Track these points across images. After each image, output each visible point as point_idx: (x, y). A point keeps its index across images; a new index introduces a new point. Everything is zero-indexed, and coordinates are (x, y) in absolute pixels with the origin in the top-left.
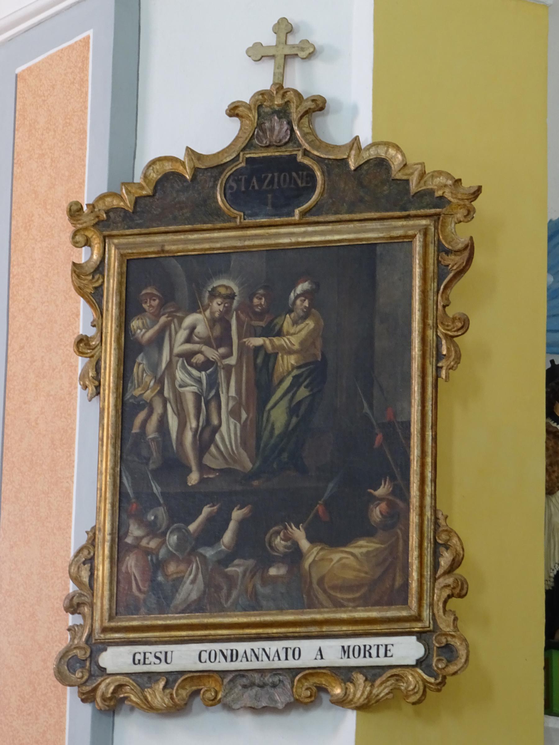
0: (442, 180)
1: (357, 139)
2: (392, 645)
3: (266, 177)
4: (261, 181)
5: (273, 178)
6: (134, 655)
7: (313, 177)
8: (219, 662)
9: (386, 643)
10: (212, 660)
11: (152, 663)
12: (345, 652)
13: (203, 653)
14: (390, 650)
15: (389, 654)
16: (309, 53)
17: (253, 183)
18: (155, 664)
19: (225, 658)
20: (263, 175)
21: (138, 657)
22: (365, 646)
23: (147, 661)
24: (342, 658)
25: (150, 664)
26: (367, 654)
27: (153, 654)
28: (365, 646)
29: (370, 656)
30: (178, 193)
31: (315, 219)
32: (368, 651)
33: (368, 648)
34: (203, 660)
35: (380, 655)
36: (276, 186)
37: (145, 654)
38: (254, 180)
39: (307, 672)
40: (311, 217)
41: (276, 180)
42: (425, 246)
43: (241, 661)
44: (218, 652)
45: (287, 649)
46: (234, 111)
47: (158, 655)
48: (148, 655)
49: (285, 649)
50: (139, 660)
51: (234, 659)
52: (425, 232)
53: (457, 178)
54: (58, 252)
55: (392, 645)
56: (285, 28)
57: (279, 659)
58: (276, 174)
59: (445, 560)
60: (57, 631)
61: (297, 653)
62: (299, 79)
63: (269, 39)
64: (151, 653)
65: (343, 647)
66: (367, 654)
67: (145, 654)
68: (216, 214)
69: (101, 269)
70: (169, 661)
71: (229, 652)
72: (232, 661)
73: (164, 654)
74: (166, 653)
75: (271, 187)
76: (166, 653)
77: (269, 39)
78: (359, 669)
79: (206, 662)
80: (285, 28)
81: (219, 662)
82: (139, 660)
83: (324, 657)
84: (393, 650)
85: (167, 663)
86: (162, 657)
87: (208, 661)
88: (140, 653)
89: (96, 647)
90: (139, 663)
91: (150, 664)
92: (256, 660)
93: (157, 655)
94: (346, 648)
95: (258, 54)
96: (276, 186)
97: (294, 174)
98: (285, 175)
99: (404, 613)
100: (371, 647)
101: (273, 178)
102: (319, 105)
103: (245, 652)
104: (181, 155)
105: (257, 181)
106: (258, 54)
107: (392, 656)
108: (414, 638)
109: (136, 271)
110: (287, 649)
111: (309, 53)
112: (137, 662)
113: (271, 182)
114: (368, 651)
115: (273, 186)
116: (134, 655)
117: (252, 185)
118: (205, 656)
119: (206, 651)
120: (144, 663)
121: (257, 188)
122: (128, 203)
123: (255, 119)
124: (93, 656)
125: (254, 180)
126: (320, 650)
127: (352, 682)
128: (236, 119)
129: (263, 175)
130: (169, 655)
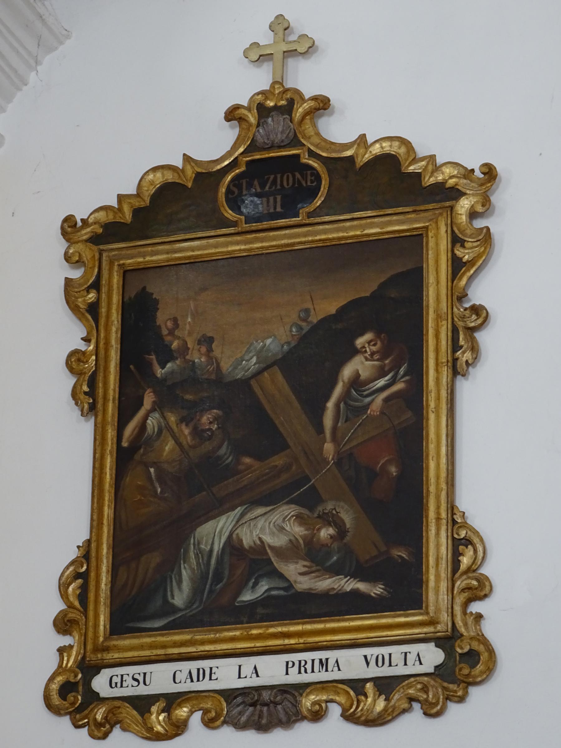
0: (448, 170)
2: (217, 667)
3: (268, 179)
5: (275, 180)
7: (318, 178)
13: (114, 678)
14: (215, 673)
15: (214, 677)
16: (308, 49)
20: (266, 177)
21: (115, 680)
22: (300, 662)
23: (125, 684)
24: (320, 671)
25: (246, 677)
26: (303, 669)
27: (131, 676)
28: (300, 662)
29: (306, 672)
31: (318, 220)
32: (304, 666)
33: (303, 663)
35: (315, 670)
36: (279, 187)
37: (122, 676)
46: (233, 114)
47: (136, 676)
49: (403, 654)
50: (116, 683)
53: (469, 168)
54: (50, 269)
55: (217, 667)
56: (281, 26)
57: (192, 681)
58: (279, 176)
59: (465, 561)
62: (307, 79)
63: (265, 38)
64: (128, 675)
66: (303, 669)
67: (122, 676)
70: (147, 683)
72: (198, 680)
73: (142, 675)
75: (274, 188)
76: (145, 674)
77: (265, 38)
80: (281, 26)
82: (116, 683)
83: (259, 675)
84: (217, 674)
85: (175, 682)
86: (141, 679)
88: (117, 676)
89: (89, 669)
90: (116, 686)
91: (246, 677)
93: (135, 677)
94: (324, 661)
95: (258, 56)
97: (298, 175)
98: (288, 177)
100: (306, 662)
101: (275, 180)
102: (322, 104)
103: (190, 673)
104: (178, 163)
105: (260, 184)
106: (258, 56)
108: (433, 644)
111: (308, 49)
112: (113, 685)
113: (274, 182)
114: (304, 666)
115: (276, 187)
120: (122, 686)
122: (128, 217)
124: (87, 681)
129: (266, 177)
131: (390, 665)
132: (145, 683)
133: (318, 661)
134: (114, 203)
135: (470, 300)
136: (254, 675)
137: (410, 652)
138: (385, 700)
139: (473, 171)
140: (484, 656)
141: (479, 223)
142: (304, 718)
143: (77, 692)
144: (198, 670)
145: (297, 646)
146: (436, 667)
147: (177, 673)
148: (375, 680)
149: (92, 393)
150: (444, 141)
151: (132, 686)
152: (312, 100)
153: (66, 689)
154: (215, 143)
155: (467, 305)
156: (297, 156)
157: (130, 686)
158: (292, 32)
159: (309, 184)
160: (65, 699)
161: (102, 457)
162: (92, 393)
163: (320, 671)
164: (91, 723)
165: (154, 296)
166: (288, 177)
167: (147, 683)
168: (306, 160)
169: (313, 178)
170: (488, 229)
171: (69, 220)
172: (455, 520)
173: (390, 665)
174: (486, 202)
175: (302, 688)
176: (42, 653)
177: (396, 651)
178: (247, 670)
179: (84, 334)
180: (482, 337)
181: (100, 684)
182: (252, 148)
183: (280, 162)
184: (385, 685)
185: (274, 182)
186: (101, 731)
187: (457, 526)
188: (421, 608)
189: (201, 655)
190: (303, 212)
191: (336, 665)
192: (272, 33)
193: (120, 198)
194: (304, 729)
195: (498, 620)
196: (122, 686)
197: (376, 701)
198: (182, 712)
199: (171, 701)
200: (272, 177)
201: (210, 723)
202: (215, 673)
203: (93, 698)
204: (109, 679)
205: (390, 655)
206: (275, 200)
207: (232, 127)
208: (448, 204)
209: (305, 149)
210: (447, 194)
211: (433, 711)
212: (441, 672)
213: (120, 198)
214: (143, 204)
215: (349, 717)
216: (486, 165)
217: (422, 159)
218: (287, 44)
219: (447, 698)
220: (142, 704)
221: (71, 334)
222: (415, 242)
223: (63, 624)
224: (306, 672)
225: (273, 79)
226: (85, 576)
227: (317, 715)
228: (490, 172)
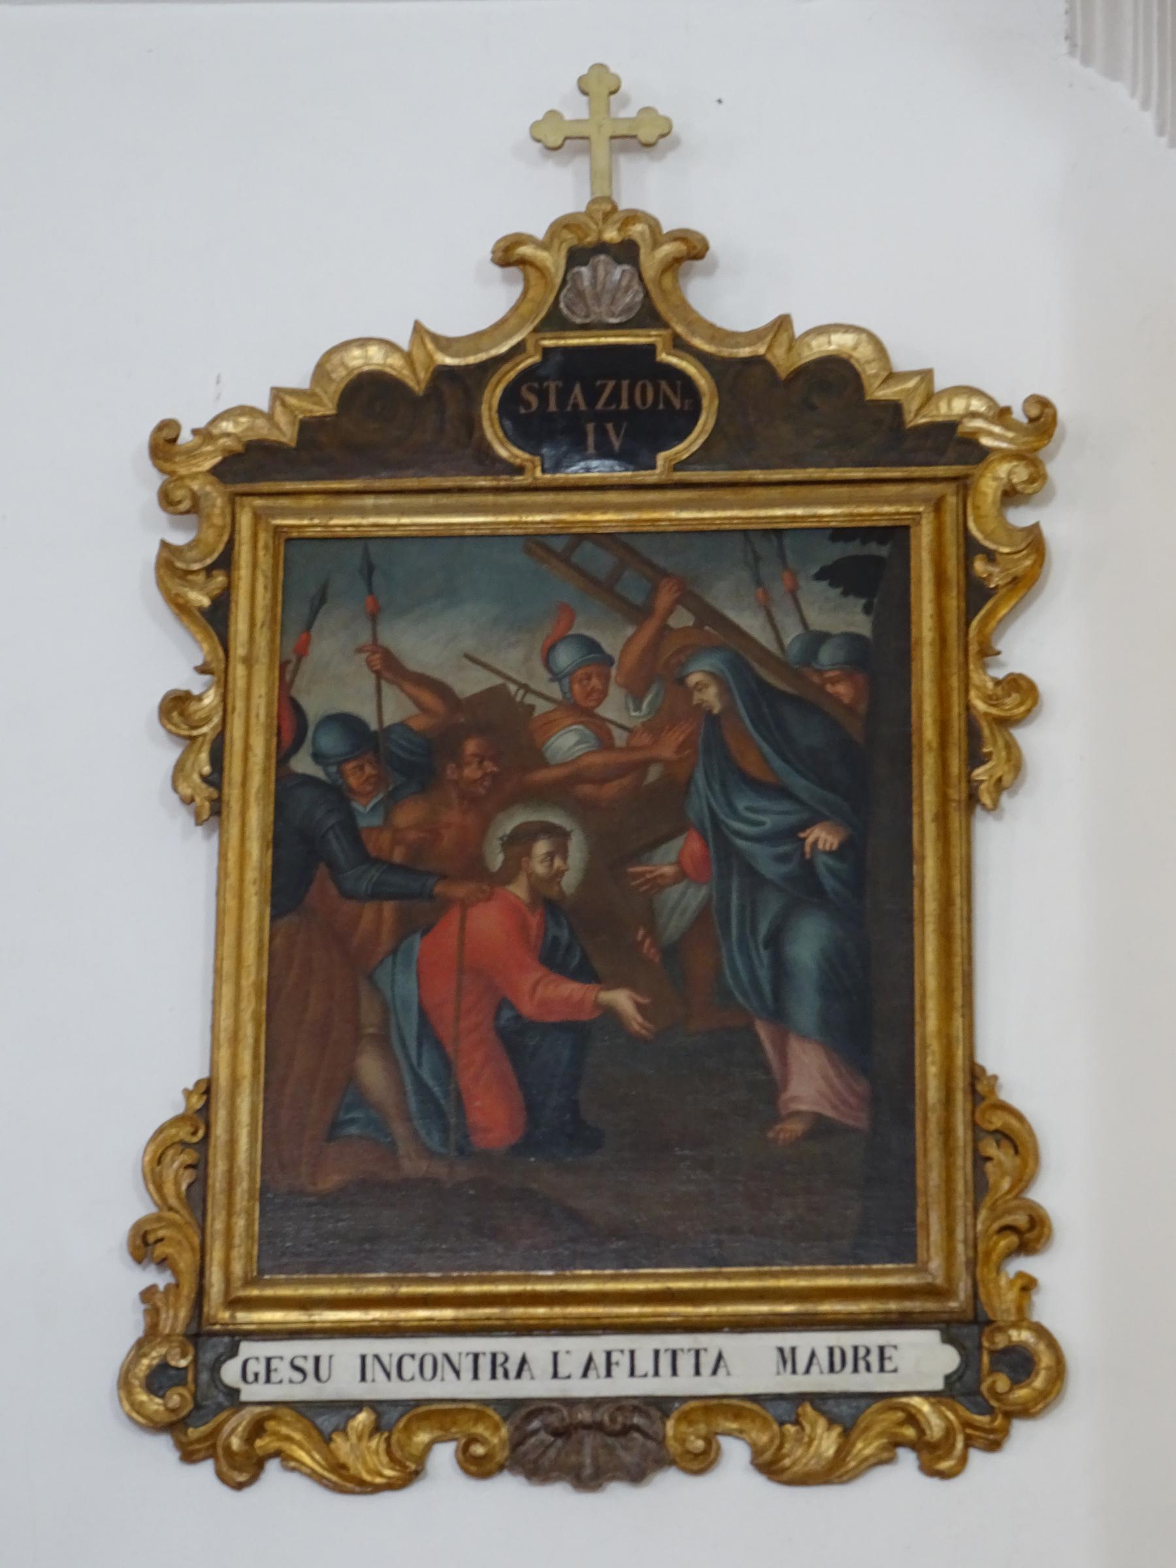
2: (895, 1347)
3: (604, 387)
4: (592, 396)
5: (617, 391)
9: (269, 1354)
12: (785, 1362)
14: (617, 1364)
15: (888, 1366)
16: (647, 138)
17: (575, 398)
18: (291, 1381)
19: (388, 1375)
21: (252, 1367)
22: (856, 1349)
23: (275, 1377)
24: (778, 1373)
28: (856, 1349)
29: (506, 1375)
30: (378, 420)
32: (502, 1364)
33: (862, 1352)
34: (562, 1371)
36: (624, 405)
38: (577, 389)
39: (693, 1404)
41: (625, 395)
42: (939, 531)
44: (440, 1359)
45: (476, 1357)
46: (508, 255)
47: (299, 1362)
48: (275, 1364)
50: (256, 1375)
52: (938, 506)
55: (895, 1347)
56: (599, 85)
58: (625, 384)
61: (787, 1358)
62: (659, 194)
63: (576, 109)
65: (781, 1350)
66: (862, 1365)
67: (268, 1361)
69: (559, 545)
74: (317, 1359)
75: (613, 407)
76: (317, 1359)
78: (817, 1399)
79: (413, 1379)
80: (599, 85)
82: (256, 1375)
84: (896, 1359)
86: (309, 1366)
95: (556, 140)
96: (624, 405)
97: (664, 385)
99: (911, 1280)
100: (868, 1352)
101: (617, 391)
102: (693, 249)
106: (556, 140)
107: (895, 1371)
111: (647, 138)
112: (250, 1377)
113: (615, 397)
117: (571, 402)
118: (410, 1367)
119: (413, 1356)
120: (268, 1380)
121: (583, 406)
122: (287, 434)
123: (557, 270)
125: (577, 389)
127: (797, 1422)
128: (514, 271)
134: (263, 404)
135: (1001, 665)
137: (705, 1350)
138: (841, 1435)
139: (1006, 411)
140: (1045, 1359)
141: (1021, 517)
142: (672, 1462)
144: (831, 1351)
146: (948, 1378)
148: (374, 1405)
149: (215, 779)
151: (291, 1381)
152: (676, 239)
153: (160, 1379)
154: (470, 305)
155: (1000, 674)
156: (651, 349)
157: (286, 1380)
158: (625, 103)
161: (946, 903)
162: (215, 779)
163: (778, 1373)
164: (220, 1451)
165: (839, 590)
166: (644, 388)
170: (1036, 526)
174: (1038, 476)
175: (661, 1405)
176: (108, 1306)
177: (538, 1348)
178: (572, 1365)
179: (199, 662)
180: (1026, 737)
182: (554, 321)
183: (610, 357)
185: (615, 397)
186: (241, 1470)
187: (983, 1105)
188: (914, 1259)
192: (585, 99)
193: (278, 394)
194: (670, 1485)
195: (1066, 1291)
196: (268, 1380)
197: (814, 1439)
199: (390, 1417)
200: (611, 384)
201: (477, 1467)
202: (617, 1364)
207: (508, 280)
210: (952, 446)
213: (278, 394)
214: (319, 411)
215: (770, 1466)
216: (1044, 403)
218: (607, 126)
219: (969, 1443)
220: (323, 1417)
221: (173, 659)
223: (143, 1245)
224: (506, 1375)
225: (592, 194)
227: (701, 1462)
228: (1042, 420)
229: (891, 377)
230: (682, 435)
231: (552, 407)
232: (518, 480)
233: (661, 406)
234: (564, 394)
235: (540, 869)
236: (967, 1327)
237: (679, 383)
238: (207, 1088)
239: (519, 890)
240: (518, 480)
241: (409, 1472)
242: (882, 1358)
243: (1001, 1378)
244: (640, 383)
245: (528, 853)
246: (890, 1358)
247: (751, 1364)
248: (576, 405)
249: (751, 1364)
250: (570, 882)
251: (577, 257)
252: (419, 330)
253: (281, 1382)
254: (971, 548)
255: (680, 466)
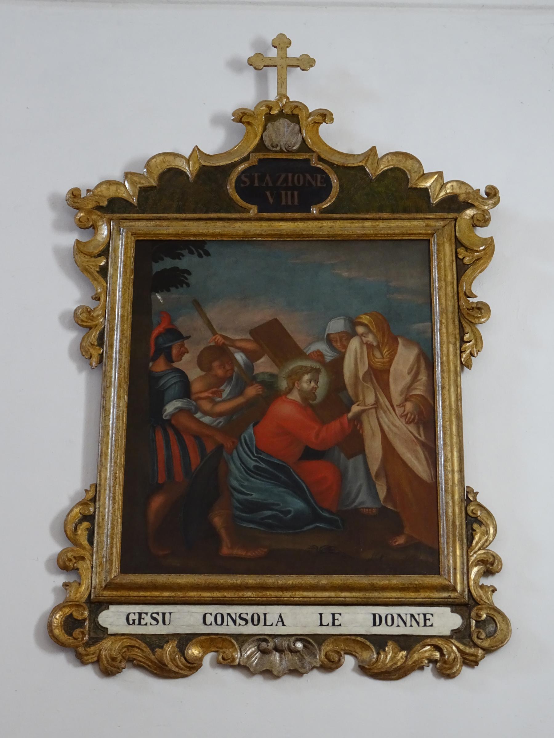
1: (373, 149)
2: (432, 615)
3: (280, 176)
5: (287, 177)
6: (128, 616)
7: (327, 180)
8: (227, 625)
10: (256, 623)
11: (149, 624)
14: (144, 619)
15: (428, 623)
18: (151, 624)
21: (132, 617)
23: (143, 622)
25: (272, 625)
27: (149, 615)
30: (172, 188)
36: (290, 184)
37: (140, 614)
40: (328, 214)
43: (277, 625)
44: (396, 617)
48: (143, 616)
50: (134, 621)
51: (378, 623)
53: (475, 189)
58: (290, 175)
60: (44, 591)
61: (376, 620)
62: (303, 91)
68: (231, 207)
70: (167, 623)
71: (422, 616)
73: (161, 614)
75: (285, 185)
76: (164, 614)
79: (211, 624)
81: (227, 625)
82: (134, 621)
84: (433, 620)
85: (129, 624)
86: (160, 618)
87: (213, 623)
89: (97, 605)
90: (134, 623)
91: (328, 625)
92: (404, 625)
95: (258, 64)
97: (308, 177)
98: (299, 177)
106: (258, 64)
109: (147, 251)
110: (406, 614)
112: (131, 622)
113: (286, 180)
116: (128, 616)
118: (210, 619)
120: (140, 624)
125: (268, 177)
126: (280, 616)
130: (167, 616)
131: (265, 624)
132: (164, 623)
133: (397, 615)
136: (280, 624)
143: (84, 627)
145: (184, 599)
147: (207, 615)
150: (447, 159)
151: (151, 624)
153: (71, 624)
154: (215, 142)
156: (307, 161)
159: (319, 184)
160: (70, 634)
166: (299, 177)
167: (166, 623)
168: (314, 162)
169: (323, 180)
171: (74, 194)
172: (468, 497)
173: (265, 624)
181: (113, 619)
184: (407, 642)
185: (286, 180)
189: (206, 600)
190: (315, 211)
191: (280, 620)
196: (140, 624)
197: (386, 659)
198: (194, 651)
202: (338, 619)
203: (100, 633)
204: (202, 617)
205: (265, 615)
206: (293, 196)
208: (451, 215)
209: (315, 155)
211: (445, 671)
212: (459, 634)
215: (366, 670)
217: (431, 174)
222: (423, 245)
226: (90, 518)
227: (330, 666)
228: (492, 193)
229: (425, 176)
230: (322, 200)
231: (256, 184)
232: (244, 215)
233: (307, 185)
234: (262, 179)
235: (305, 386)
236: (465, 605)
237: (319, 176)
238: (95, 487)
239: (295, 396)
240: (244, 215)
241: (193, 666)
242: (425, 620)
243: (481, 631)
244: (296, 175)
245: (300, 379)
246: (429, 619)
247: (357, 620)
248: (267, 184)
249: (357, 620)
250: (320, 393)
251: (270, 118)
252: (196, 149)
253: (146, 624)
254: (458, 243)
255: (326, 211)
